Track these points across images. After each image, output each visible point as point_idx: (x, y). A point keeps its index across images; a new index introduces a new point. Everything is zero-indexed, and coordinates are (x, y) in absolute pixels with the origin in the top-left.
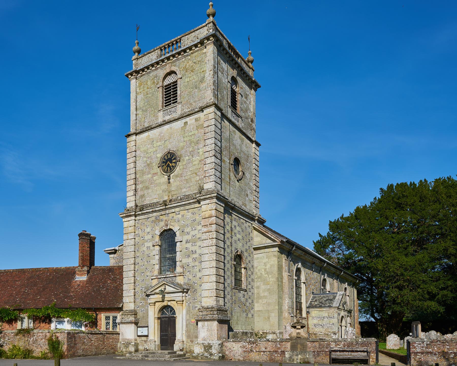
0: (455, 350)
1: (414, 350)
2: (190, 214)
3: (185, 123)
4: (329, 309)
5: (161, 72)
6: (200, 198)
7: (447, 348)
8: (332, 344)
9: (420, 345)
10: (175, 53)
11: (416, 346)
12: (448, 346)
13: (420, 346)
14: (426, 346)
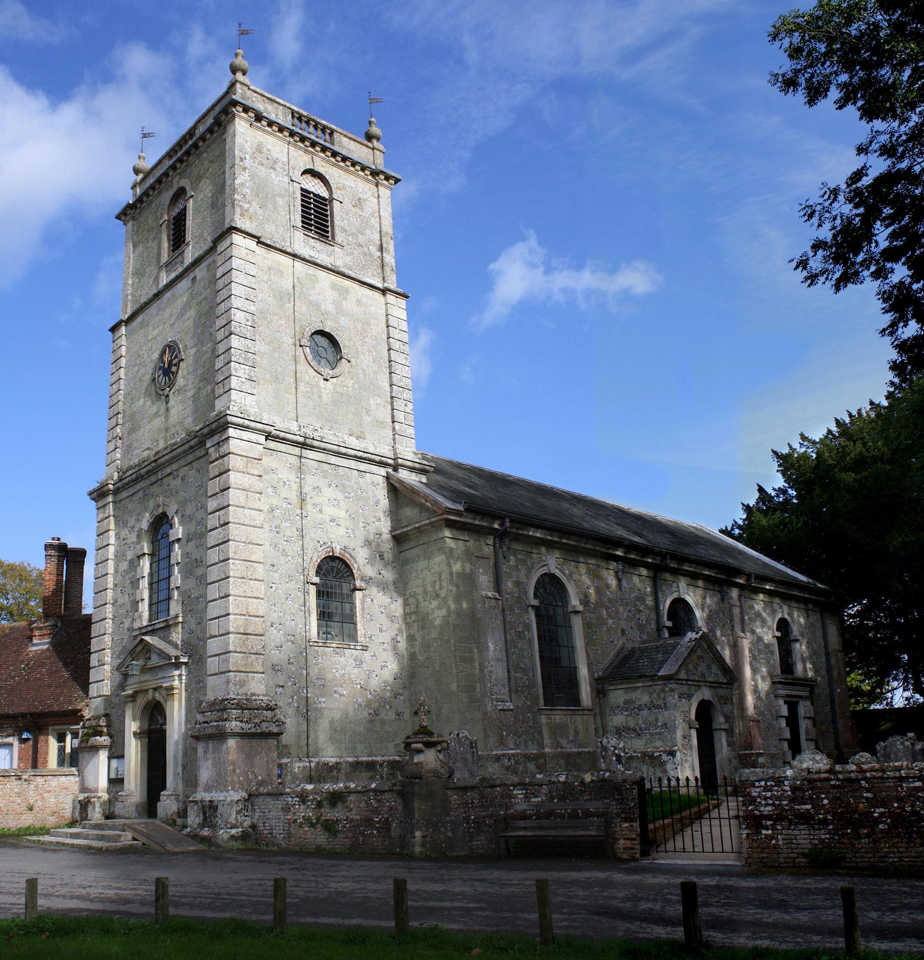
0: (896, 805)
1: (752, 810)
2: (193, 472)
3: (193, 279)
4: (651, 683)
5: (168, 195)
6: (202, 432)
7: (867, 798)
8: (515, 792)
9: (770, 790)
10: (182, 155)
11: (756, 794)
12: (868, 790)
13: (769, 794)
14: (789, 793)
